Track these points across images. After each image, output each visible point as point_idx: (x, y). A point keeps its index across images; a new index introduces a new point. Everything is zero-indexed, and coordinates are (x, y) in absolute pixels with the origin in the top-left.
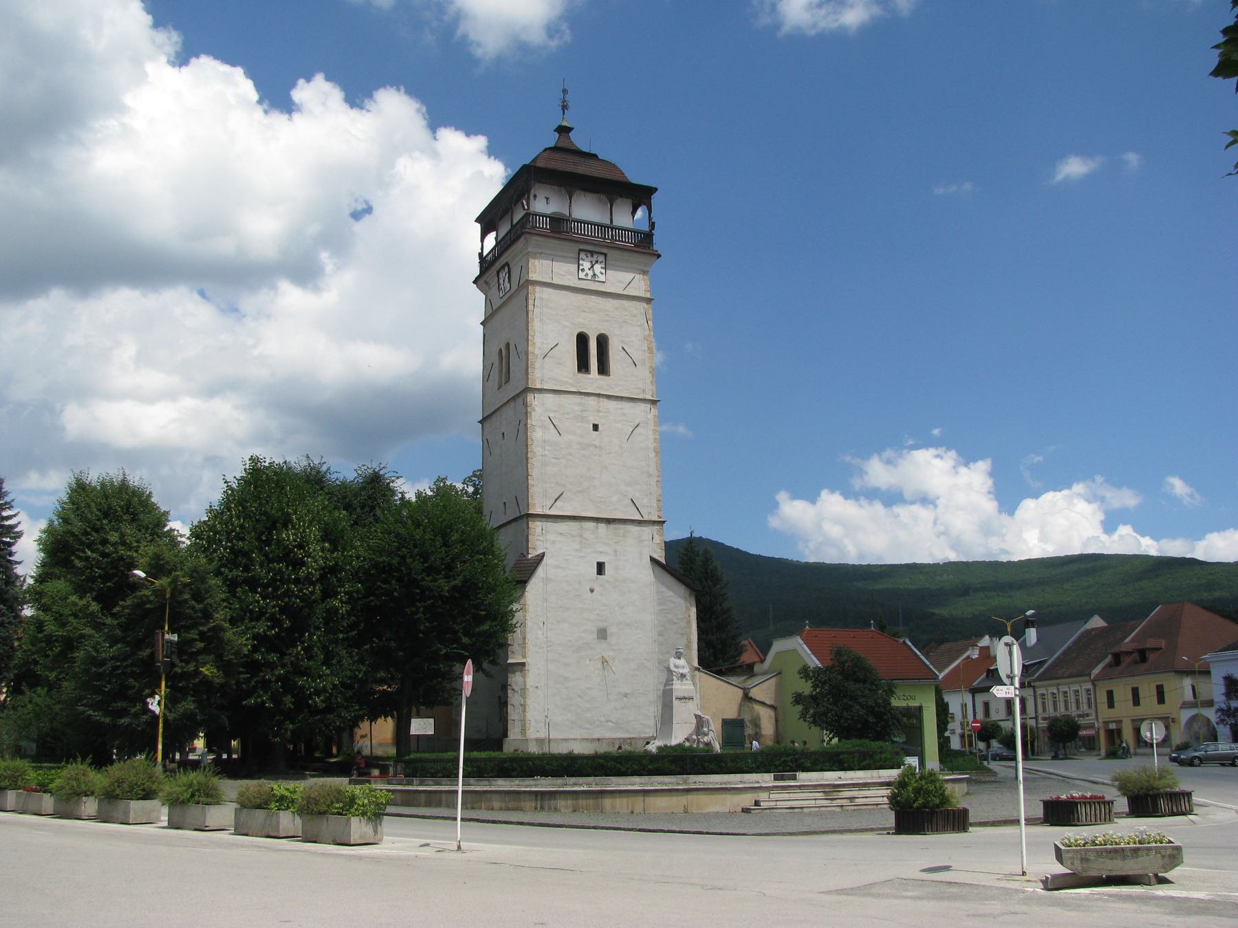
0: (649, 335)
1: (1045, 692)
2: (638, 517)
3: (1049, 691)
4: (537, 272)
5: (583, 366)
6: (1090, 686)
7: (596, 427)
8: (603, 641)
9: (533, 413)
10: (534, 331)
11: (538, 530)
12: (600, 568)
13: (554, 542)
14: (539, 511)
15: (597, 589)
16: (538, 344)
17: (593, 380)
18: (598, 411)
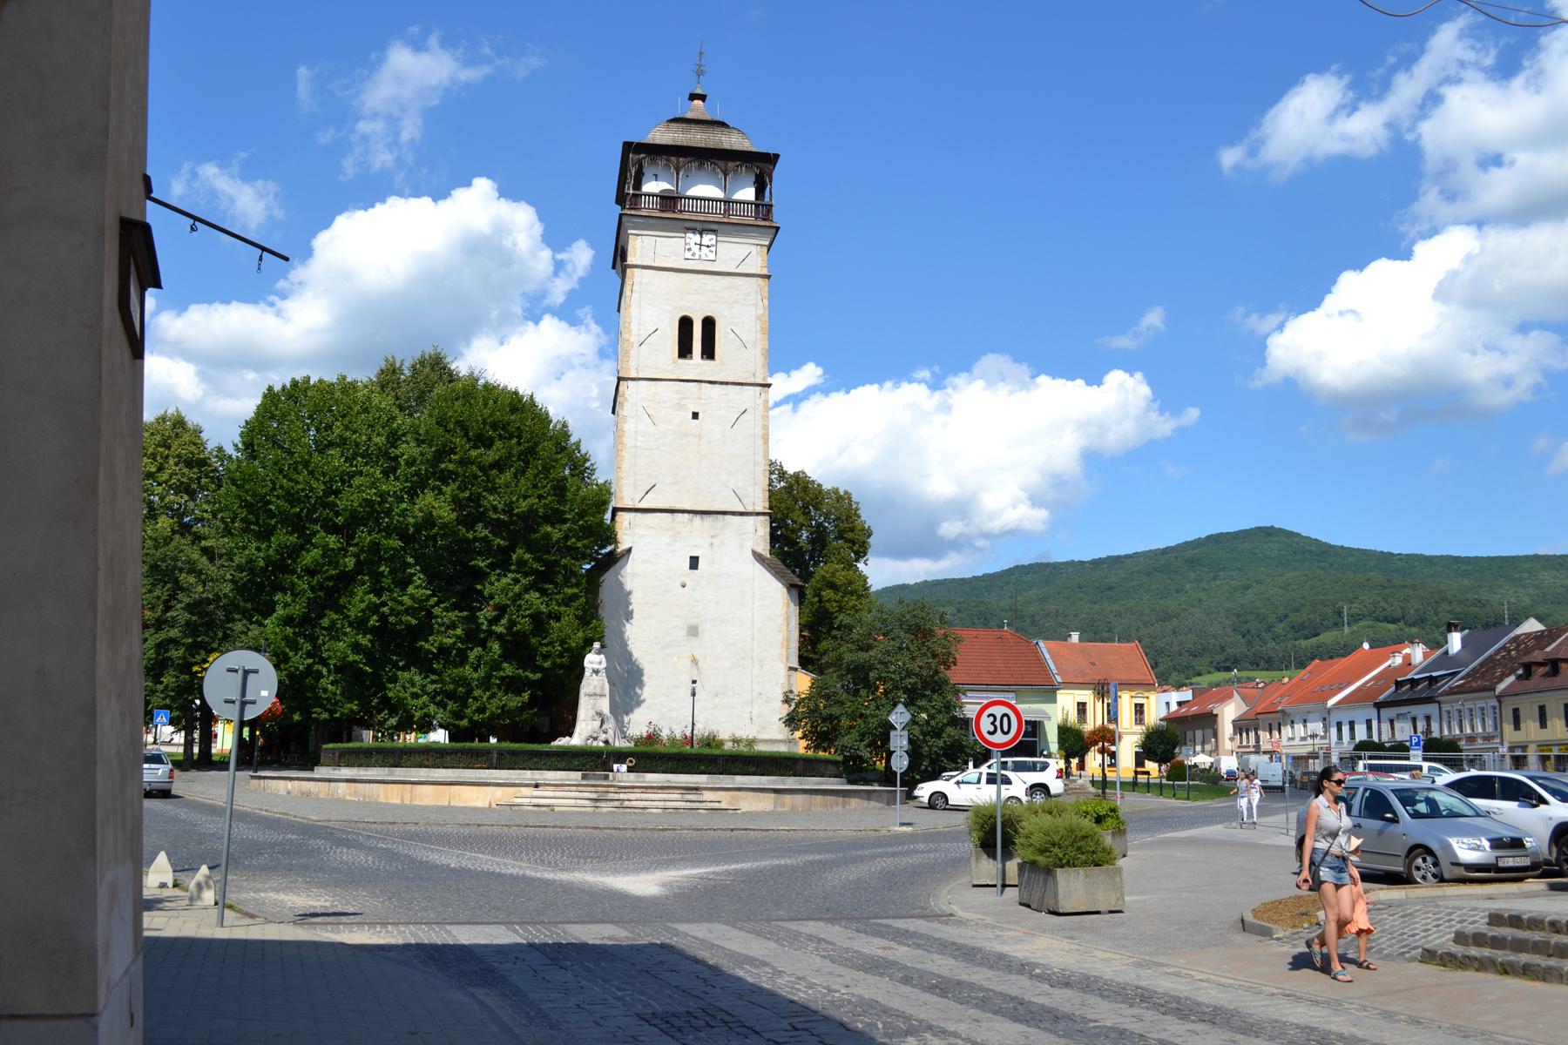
0: (763, 314)
1: (1484, 705)
2: (741, 509)
3: (1478, 706)
4: (638, 254)
5: (685, 350)
6: (1496, 703)
7: (695, 415)
8: (693, 638)
9: (625, 404)
11: (626, 524)
12: (694, 562)
13: (642, 536)
16: (634, 327)
17: (696, 365)
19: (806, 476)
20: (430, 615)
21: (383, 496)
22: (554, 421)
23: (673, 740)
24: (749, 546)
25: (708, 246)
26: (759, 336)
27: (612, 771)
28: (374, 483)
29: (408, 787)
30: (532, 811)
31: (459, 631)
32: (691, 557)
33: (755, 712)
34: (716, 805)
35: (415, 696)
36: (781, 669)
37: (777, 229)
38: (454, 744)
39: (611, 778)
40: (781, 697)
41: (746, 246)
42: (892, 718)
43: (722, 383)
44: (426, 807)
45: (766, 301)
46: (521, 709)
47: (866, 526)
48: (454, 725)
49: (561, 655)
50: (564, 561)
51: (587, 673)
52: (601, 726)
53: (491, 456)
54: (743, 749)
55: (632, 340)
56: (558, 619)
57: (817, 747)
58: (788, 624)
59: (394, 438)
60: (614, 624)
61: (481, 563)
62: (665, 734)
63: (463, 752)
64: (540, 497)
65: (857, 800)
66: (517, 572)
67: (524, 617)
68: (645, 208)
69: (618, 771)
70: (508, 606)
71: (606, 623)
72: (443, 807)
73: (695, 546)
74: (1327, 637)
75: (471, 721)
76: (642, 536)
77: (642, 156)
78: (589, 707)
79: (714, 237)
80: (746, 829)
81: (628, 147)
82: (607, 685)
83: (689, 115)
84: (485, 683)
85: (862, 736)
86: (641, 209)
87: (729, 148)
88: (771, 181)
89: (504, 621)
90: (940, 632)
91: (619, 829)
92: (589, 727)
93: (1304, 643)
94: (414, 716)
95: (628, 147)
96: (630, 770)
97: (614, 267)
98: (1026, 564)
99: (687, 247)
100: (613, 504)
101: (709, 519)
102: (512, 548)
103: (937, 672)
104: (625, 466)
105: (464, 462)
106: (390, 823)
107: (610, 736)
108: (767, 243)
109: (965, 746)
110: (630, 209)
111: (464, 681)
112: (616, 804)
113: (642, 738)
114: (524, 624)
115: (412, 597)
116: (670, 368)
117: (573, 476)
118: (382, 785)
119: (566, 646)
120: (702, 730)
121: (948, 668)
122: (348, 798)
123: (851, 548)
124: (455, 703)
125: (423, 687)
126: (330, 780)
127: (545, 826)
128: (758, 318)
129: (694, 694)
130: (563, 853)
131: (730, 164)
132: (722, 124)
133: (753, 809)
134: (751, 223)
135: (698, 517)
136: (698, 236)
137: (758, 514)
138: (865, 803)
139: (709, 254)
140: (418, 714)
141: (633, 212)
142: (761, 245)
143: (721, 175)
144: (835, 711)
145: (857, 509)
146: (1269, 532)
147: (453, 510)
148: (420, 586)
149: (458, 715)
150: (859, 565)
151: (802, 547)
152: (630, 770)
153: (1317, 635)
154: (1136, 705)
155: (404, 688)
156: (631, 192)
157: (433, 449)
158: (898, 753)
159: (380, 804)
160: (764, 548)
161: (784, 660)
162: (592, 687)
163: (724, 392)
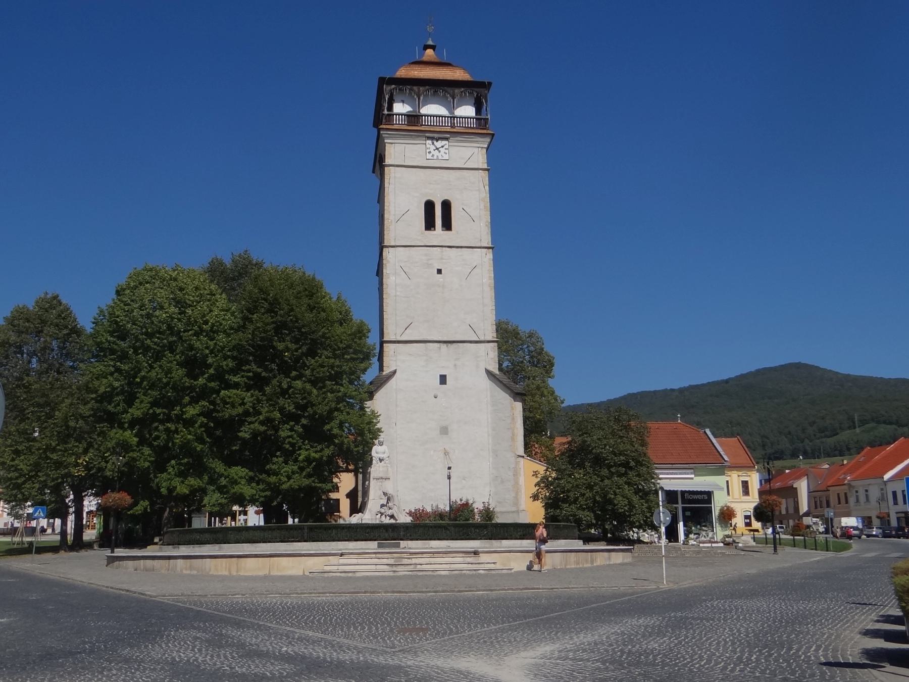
2: (476, 339)
5: (430, 224)
10: (389, 203)
11: (392, 353)
12: (443, 379)
14: (393, 338)
15: (439, 395)
16: (392, 212)
18: (442, 259)
25: (442, 147)
32: (441, 376)
43: (457, 247)
45: (487, 188)
68: (396, 124)
73: (443, 367)
74: (845, 436)
77: (393, 86)
81: (382, 81)
83: (425, 58)
86: (393, 125)
88: (486, 102)
93: (830, 440)
95: (382, 81)
97: (374, 172)
99: (428, 151)
108: (486, 146)
112: (412, 567)
122: (185, 572)
126: (169, 558)
129: (449, 478)
131: (457, 91)
137: (489, 342)
142: (482, 148)
143: (450, 99)
146: (798, 366)
153: (837, 434)
154: (743, 482)
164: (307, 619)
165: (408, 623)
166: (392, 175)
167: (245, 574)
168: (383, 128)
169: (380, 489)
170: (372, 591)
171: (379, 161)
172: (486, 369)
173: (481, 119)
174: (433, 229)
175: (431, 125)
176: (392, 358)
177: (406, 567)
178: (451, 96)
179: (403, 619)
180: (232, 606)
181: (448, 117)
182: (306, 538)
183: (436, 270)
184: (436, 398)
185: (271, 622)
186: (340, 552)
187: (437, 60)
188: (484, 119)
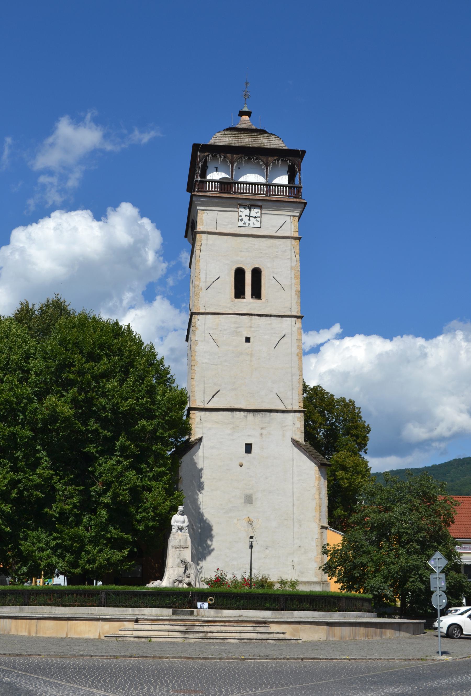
2: (282, 408)
7: (248, 340)
8: (248, 505)
9: (197, 332)
11: (198, 420)
12: (249, 448)
13: (210, 429)
14: (199, 404)
16: (202, 276)
19: (322, 389)
20: (54, 489)
21: (20, 399)
22: (145, 345)
23: (236, 583)
24: (289, 435)
25: (255, 217)
26: (294, 281)
27: (196, 608)
28: (12, 388)
29: (34, 621)
30: (133, 642)
31: (75, 500)
33: (296, 560)
34: (281, 636)
35: (41, 550)
36: (315, 528)
37: (305, 204)
38: (70, 586)
39: (195, 613)
40: (320, 549)
41: (282, 217)
42: (431, 563)
43: (267, 316)
44: (48, 638)
45: (298, 256)
46: (121, 562)
47: (366, 425)
48: (70, 572)
49: (153, 519)
50: (154, 447)
51: (174, 530)
52: (185, 572)
53: (101, 367)
54: (288, 589)
55: (200, 285)
56: (150, 490)
57: (350, 588)
58: (320, 493)
59: (27, 357)
60: (190, 493)
61: (92, 449)
62: (229, 577)
63: (78, 592)
64: (138, 399)
65: (391, 630)
66: (120, 456)
67: (124, 490)
68: (209, 191)
69: (201, 608)
70: (113, 482)
71: (184, 494)
72: (62, 638)
73: (249, 436)
75: (83, 568)
76: (210, 429)
77: (206, 154)
78: (176, 556)
79: (259, 210)
80: (313, 659)
81: (196, 147)
82: (189, 539)
83: (239, 126)
84: (94, 541)
85: (386, 579)
86: (206, 191)
87: (269, 147)
88: (300, 170)
89: (110, 494)
90: (440, 498)
91: (208, 659)
92: (176, 573)
94: (40, 565)
95: (196, 147)
96: (210, 607)
97: (186, 236)
98: (462, 458)
99: (240, 218)
100: (188, 406)
101: (259, 416)
102: (116, 438)
103: (441, 528)
104: (197, 377)
105: (81, 373)
106: (17, 655)
107: (192, 579)
108: (298, 214)
109: (465, 587)
110: (198, 191)
111: (77, 538)
112: (201, 635)
113: (212, 580)
114: (126, 496)
115: (40, 476)
116: (229, 305)
117: (159, 384)
118: (14, 620)
119: (158, 512)
120: (257, 574)
121: (449, 525)
123: (355, 441)
124: (72, 555)
125: (47, 543)
127: (146, 657)
128: (292, 268)
129: (251, 547)
130: (167, 686)
131: (270, 159)
132: (263, 132)
133: (310, 639)
134: (286, 200)
135: (251, 414)
136: (248, 210)
137: (295, 411)
138: (397, 634)
139: (256, 222)
140: (43, 563)
141: (201, 194)
142: (294, 216)
143: (264, 167)
144: (365, 559)
145: (359, 413)
147: (71, 408)
148: (46, 467)
149: (74, 565)
150: (361, 453)
151: (320, 441)
152: (210, 607)
155: (33, 544)
156: (199, 179)
157: (57, 363)
158: (438, 592)
159: (11, 636)
160: (300, 437)
161: (318, 521)
162: (178, 540)
163: (269, 322)
164: (94, 679)
165: (185, 685)
166: (204, 242)
167: (44, 636)
168: (196, 195)
169: (178, 558)
170: (160, 656)
171: (192, 227)
172: (292, 439)
173: (294, 187)
174: (242, 296)
175: (243, 193)
176: (198, 426)
177: (198, 635)
178: (264, 163)
179: (182, 682)
180: (28, 664)
181: (264, 185)
182: (103, 603)
183: (245, 339)
184: (241, 466)
185: (62, 680)
186: (135, 618)
187: (253, 127)
188: (297, 187)
